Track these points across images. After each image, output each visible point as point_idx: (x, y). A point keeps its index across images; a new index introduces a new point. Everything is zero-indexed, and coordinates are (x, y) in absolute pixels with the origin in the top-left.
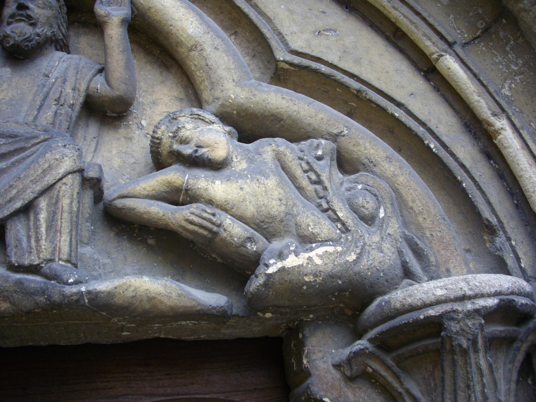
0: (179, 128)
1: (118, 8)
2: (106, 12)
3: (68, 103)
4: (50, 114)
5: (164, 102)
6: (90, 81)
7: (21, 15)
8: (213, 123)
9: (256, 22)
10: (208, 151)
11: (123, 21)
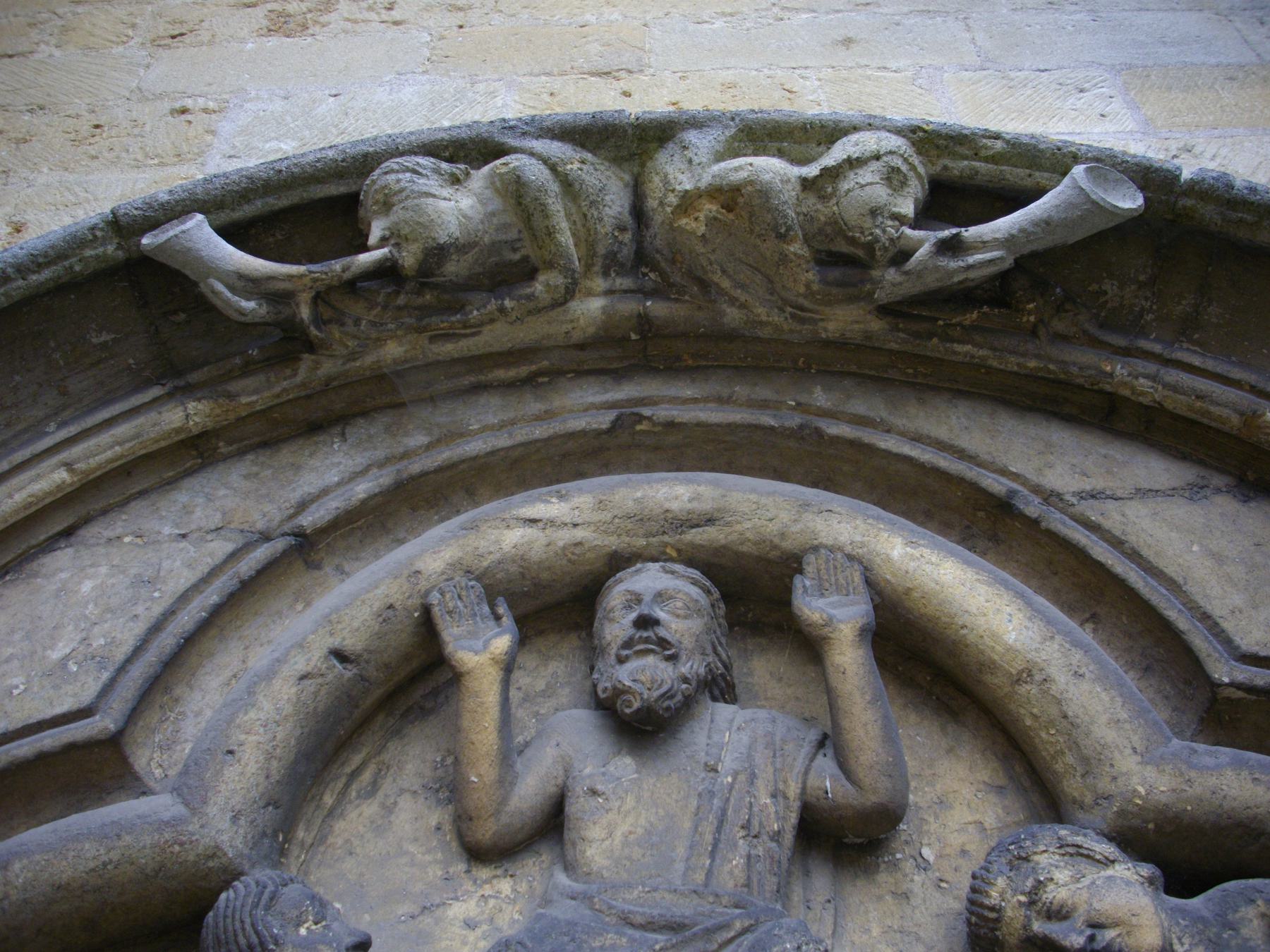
0: (1040, 882)
1: (844, 599)
2: (825, 616)
3: (767, 829)
4: (738, 861)
5: (965, 798)
6: (806, 772)
7: (647, 640)
8: (1113, 862)
9: (1148, 596)
10: (1119, 935)
11: (863, 631)
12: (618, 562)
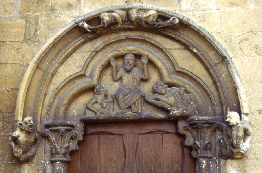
4: (135, 83)
12: (126, 54)
